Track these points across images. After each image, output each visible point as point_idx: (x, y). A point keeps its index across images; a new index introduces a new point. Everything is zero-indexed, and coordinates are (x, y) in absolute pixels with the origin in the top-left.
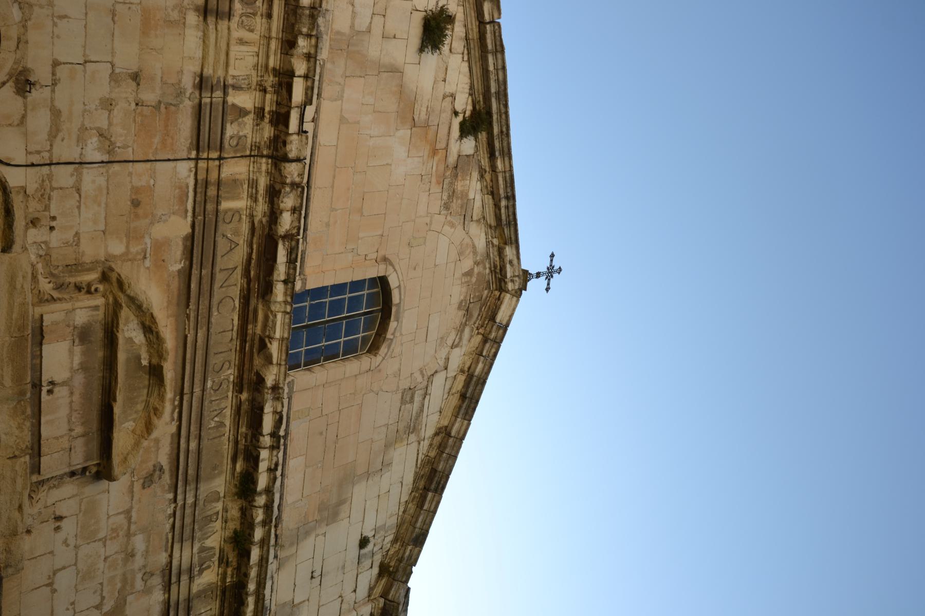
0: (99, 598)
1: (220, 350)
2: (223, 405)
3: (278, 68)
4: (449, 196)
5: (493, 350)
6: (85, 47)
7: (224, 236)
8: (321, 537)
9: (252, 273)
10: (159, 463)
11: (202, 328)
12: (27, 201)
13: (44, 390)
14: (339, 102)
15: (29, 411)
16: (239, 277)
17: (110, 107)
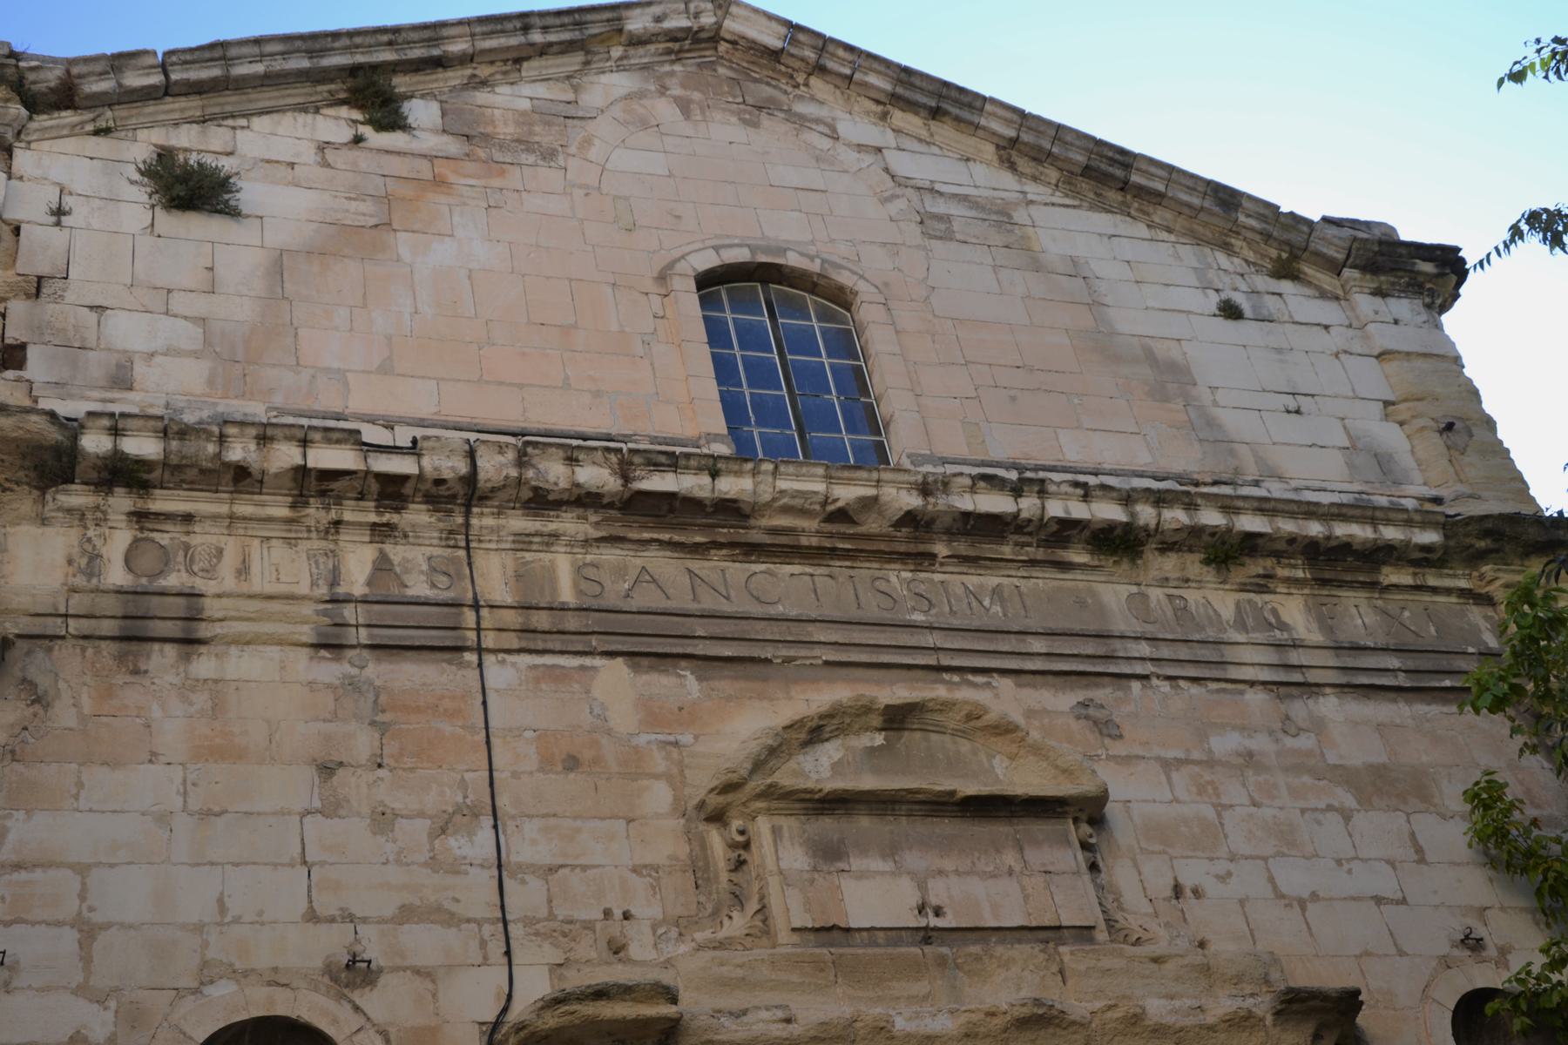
0: (1329, 815)
3: (290, 499)
4: (527, 150)
5: (840, 52)
6: (275, 865)
8: (1220, 395)
9: (699, 539)
10: (1072, 708)
12: (577, 961)
13: (934, 922)
15: (975, 949)
17: (389, 816)
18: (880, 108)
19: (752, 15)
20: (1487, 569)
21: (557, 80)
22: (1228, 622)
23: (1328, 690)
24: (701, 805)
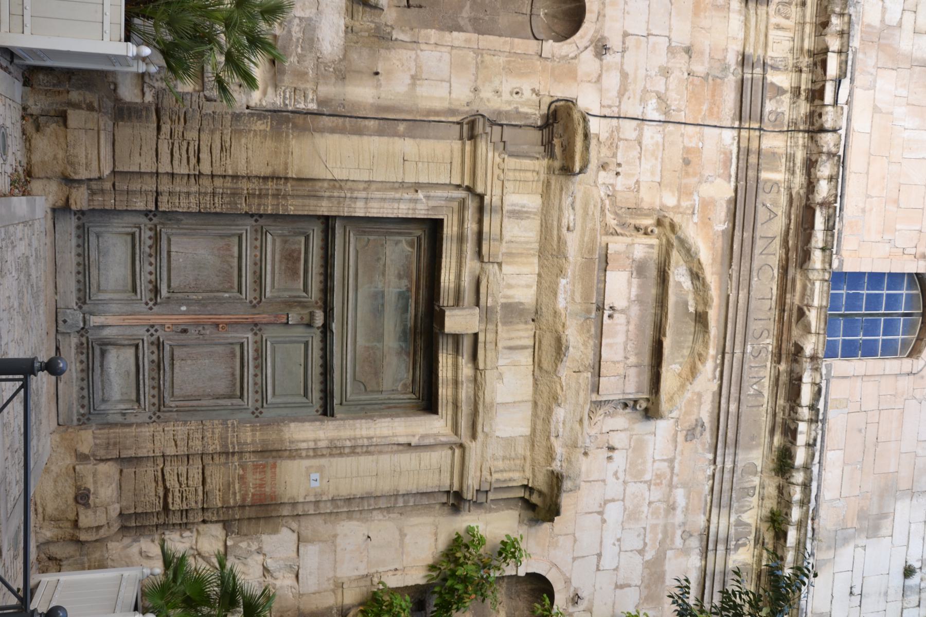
0: (642, 542)
1: (760, 317)
3: (812, 49)
6: (648, 22)
7: (764, 205)
9: (791, 243)
10: (701, 418)
11: (743, 290)
12: (600, 147)
13: (607, 313)
14: (872, 91)
15: (593, 330)
16: (778, 247)
17: (667, 74)
22: (740, 516)
23: (703, 563)
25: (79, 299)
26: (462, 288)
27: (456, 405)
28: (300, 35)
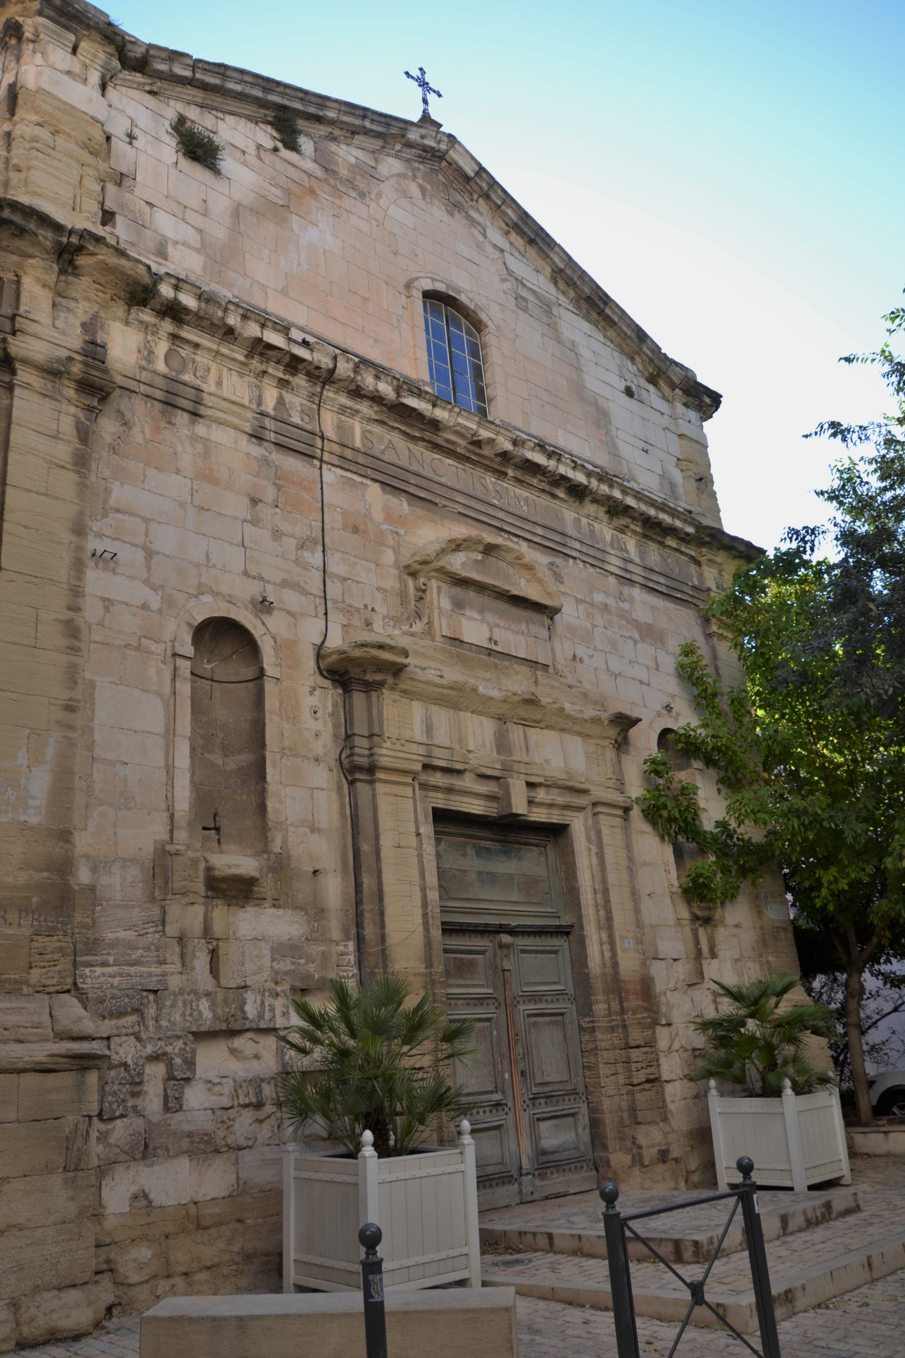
2: (513, 494)
5: (499, 191)
8: (619, 432)
9: (417, 434)
13: (494, 647)
18: (506, 228)
19: (464, 153)
20: (704, 550)
21: (368, 151)
24: (407, 567)
25: (510, 1182)
26: (488, 793)
27: (566, 807)
28: (288, 960)
